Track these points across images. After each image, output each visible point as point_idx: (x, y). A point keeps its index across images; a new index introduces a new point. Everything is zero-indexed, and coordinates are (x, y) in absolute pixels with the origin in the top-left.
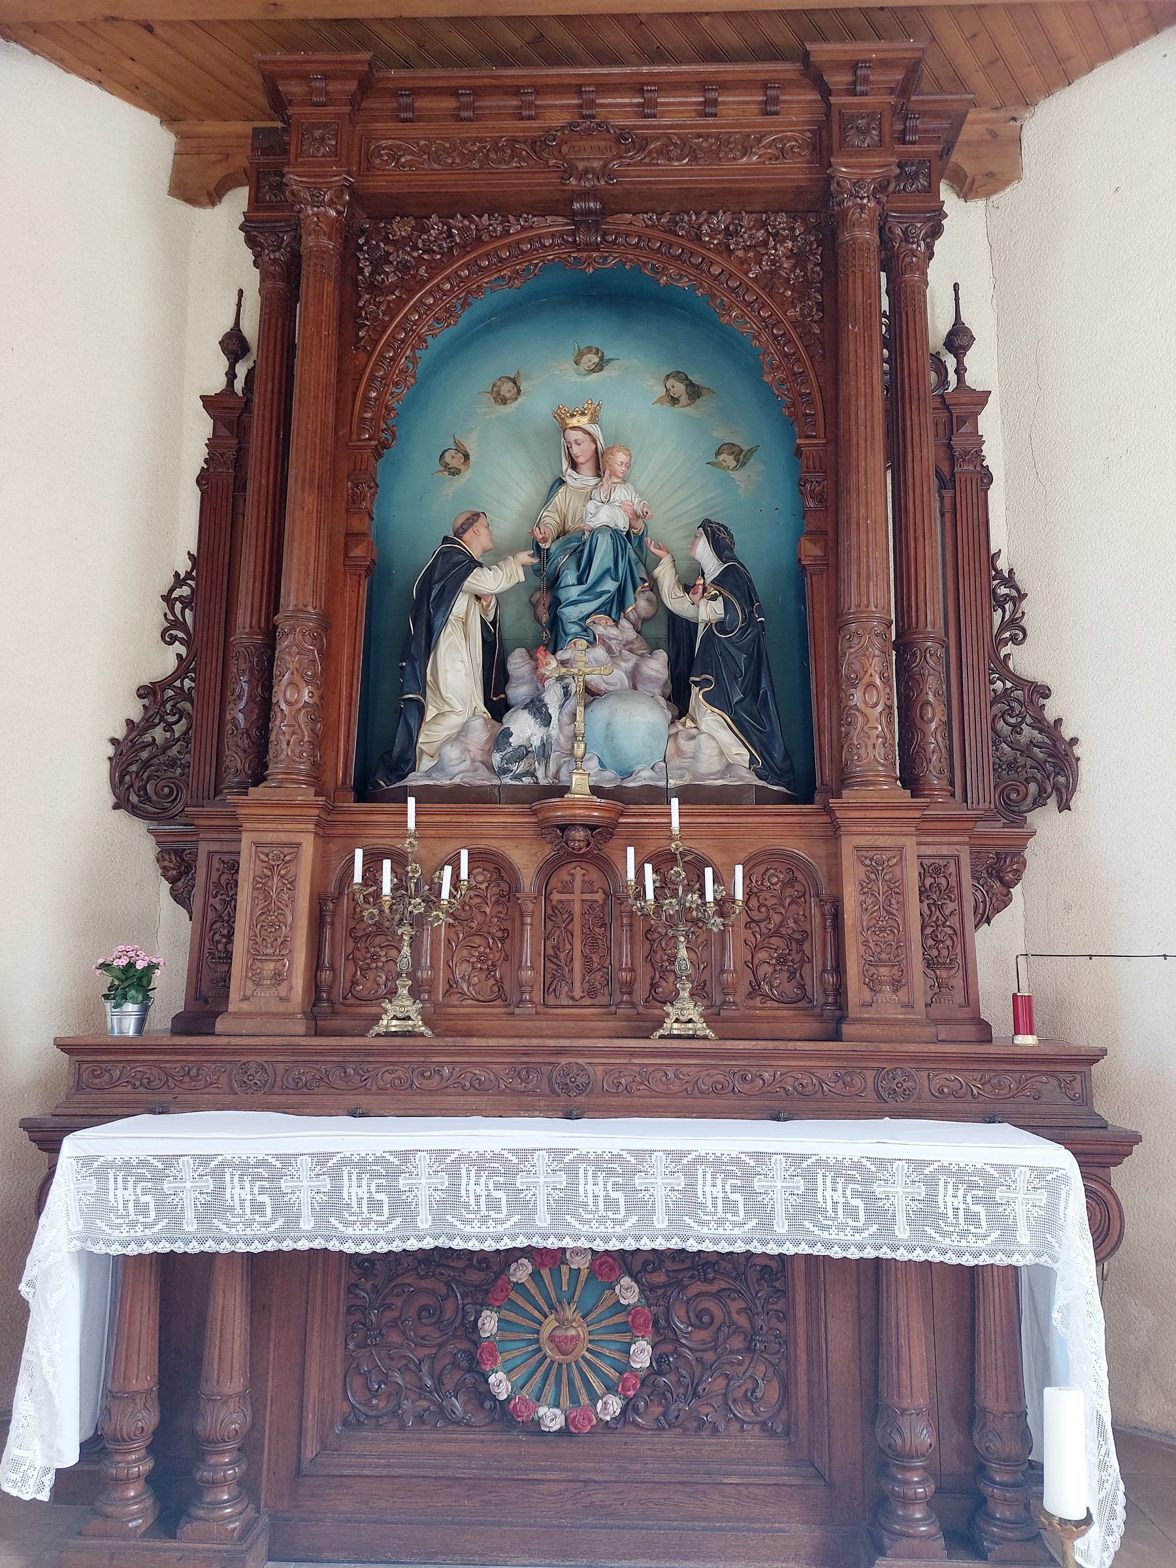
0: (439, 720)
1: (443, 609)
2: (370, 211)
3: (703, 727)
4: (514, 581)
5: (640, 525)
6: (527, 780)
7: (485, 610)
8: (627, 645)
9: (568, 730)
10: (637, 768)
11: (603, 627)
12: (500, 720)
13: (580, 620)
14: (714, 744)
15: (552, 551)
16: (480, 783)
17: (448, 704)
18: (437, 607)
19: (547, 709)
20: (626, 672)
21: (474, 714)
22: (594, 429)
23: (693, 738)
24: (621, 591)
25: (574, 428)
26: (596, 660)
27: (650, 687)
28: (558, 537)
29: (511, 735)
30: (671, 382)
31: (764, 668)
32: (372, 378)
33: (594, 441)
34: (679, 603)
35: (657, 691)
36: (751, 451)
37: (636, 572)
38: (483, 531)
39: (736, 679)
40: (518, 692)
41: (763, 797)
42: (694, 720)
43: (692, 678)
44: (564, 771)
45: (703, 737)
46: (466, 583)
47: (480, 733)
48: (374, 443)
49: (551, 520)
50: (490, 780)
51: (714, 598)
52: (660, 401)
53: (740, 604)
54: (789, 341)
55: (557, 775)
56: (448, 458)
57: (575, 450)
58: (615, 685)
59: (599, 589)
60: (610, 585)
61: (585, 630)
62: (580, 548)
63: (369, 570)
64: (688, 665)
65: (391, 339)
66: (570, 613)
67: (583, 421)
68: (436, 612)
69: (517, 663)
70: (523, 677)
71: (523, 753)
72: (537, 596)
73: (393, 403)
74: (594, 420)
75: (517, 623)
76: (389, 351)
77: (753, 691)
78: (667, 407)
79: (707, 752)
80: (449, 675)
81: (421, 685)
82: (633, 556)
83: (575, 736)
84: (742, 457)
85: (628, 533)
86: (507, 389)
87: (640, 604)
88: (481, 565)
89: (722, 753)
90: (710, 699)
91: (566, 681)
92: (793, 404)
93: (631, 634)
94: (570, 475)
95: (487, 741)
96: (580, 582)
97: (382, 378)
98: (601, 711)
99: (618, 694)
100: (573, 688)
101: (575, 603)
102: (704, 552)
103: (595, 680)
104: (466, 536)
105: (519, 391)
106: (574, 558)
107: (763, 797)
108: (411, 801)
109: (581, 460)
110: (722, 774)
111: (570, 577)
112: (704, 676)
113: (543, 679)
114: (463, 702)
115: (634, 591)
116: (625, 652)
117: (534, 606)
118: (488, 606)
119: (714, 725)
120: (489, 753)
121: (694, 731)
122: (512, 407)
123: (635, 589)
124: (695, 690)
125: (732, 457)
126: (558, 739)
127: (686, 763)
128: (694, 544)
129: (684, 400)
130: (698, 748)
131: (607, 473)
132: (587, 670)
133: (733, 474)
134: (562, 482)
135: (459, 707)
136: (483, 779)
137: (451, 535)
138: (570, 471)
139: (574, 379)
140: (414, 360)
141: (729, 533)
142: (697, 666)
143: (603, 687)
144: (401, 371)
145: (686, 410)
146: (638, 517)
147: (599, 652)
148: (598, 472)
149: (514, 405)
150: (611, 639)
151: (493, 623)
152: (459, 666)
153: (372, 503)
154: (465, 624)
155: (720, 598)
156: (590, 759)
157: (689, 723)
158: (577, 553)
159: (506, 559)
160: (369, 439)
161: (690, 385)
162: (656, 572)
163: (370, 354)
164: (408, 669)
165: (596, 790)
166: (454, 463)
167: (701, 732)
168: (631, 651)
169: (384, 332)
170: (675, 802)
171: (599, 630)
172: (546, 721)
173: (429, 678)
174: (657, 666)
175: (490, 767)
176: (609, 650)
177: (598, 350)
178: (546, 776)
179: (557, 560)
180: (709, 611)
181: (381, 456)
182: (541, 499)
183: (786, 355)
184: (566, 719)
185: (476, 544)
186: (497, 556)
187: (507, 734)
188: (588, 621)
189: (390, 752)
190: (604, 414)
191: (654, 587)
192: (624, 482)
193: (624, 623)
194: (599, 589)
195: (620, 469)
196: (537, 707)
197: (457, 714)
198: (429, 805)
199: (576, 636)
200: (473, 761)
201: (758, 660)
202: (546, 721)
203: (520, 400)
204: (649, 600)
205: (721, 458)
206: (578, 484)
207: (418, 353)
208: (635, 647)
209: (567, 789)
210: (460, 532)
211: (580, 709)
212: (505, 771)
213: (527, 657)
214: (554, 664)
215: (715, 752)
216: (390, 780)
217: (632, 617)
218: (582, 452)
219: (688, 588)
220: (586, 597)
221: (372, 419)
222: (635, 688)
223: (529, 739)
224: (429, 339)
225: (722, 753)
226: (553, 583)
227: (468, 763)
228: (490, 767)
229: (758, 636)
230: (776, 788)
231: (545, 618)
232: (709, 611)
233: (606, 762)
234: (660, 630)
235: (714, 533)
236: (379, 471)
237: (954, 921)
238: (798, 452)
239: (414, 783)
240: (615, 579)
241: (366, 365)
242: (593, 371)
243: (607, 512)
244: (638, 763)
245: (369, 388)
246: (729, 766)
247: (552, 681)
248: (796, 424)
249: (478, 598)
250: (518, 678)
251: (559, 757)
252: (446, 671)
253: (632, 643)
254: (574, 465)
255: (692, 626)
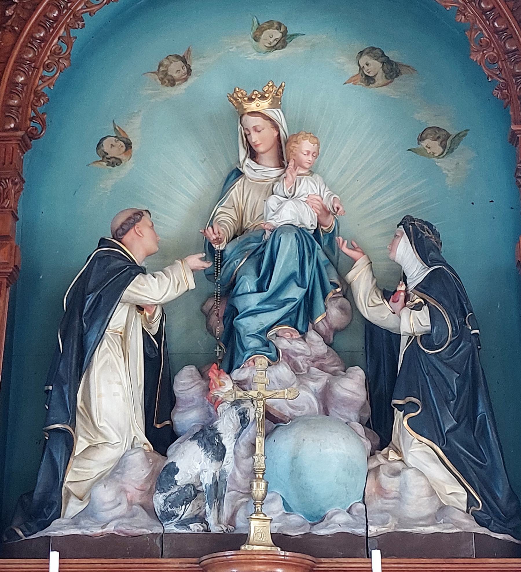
0: (91, 453)
1: (98, 323)
2: (272, 232)
3: (409, 460)
4: (182, 290)
5: (330, 221)
6: (195, 527)
7: (148, 322)
8: (317, 361)
9: (246, 464)
10: (330, 511)
11: (287, 341)
12: (164, 454)
13: (261, 332)
14: (423, 482)
15: (227, 253)
16: (137, 531)
17: (102, 434)
18: (91, 322)
19: (220, 440)
20: (315, 394)
21: (133, 446)
22: (276, 114)
23: (397, 473)
24: (309, 299)
25: (253, 113)
26: (279, 381)
27: (344, 411)
28: (235, 237)
29: (177, 471)
30: (365, 59)
31: (481, 390)
32: (20, 61)
33: (276, 127)
34: (377, 312)
35: (353, 416)
36: (460, 136)
37: (326, 276)
38: (147, 232)
39: (447, 402)
40: (186, 418)
41: (484, 548)
42: (398, 451)
43: (395, 401)
44: (241, 515)
45: (409, 473)
46: (126, 293)
47: (139, 469)
48: (20, 133)
49: (226, 217)
50: (149, 527)
51: (418, 307)
52: (352, 80)
53: (449, 314)
54: (499, 16)
55: (232, 521)
56: (106, 147)
57: (254, 138)
58: (302, 408)
59: (282, 297)
60: (295, 292)
61: (266, 344)
62: (259, 247)
63: (11, 278)
64: (390, 385)
65: (42, 18)
66: (249, 325)
67: (263, 106)
68: (90, 327)
69: (186, 383)
70: (193, 400)
71: (192, 493)
72: (210, 303)
73: (44, 88)
74: (276, 103)
75: (184, 335)
76: (39, 31)
77: (468, 416)
78: (360, 87)
79: (415, 491)
80: (104, 400)
81: (70, 414)
82: (323, 258)
83: (254, 472)
84: (449, 143)
85: (316, 231)
86: (175, 69)
87: (329, 314)
88: (143, 271)
89: (433, 493)
90: (416, 426)
91: (243, 406)
92: (507, 86)
93: (321, 348)
94: (248, 166)
95: (148, 480)
96: (260, 289)
97: (31, 60)
98: (285, 442)
99: (305, 420)
100: (251, 414)
101: (254, 313)
102: (405, 254)
103: (280, 405)
104: (127, 238)
105: (189, 71)
106: (253, 260)
107: (484, 548)
108: (54, 556)
109: (261, 149)
110: (434, 519)
111: (248, 283)
112: (408, 399)
113: (216, 402)
114: (120, 431)
115: (324, 297)
116: (314, 370)
117: (207, 316)
118: (152, 317)
119: (422, 458)
120: (150, 493)
121: (399, 465)
122: (180, 89)
123: (325, 297)
124: (398, 414)
125: (437, 143)
126: (234, 475)
127: (390, 504)
128: (393, 245)
129: (380, 79)
130: (403, 487)
131: (292, 163)
132: (268, 393)
133: (441, 163)
134: (239, 174)
135: (114, 438)
136: (142, 526)
137: (109, 236)
138: (248, 161)
139: (252, 57)
140: (68, 40)
141: (434, 231)
142: (401, 386)
143: (288, 411)
144: (53, 53)
145: (381, 90)
146: (329, 213)
147: (283, 371)
148: (281, 162)
149: (184, 86)
150: (296, 354)
151: (158, 336)
152: (117, 388)
153: (16, 200)
154: (124, 339)
155: (426, 308)
156: (272, 500)
157: (392, 456)
158: (256, 255)
159: (172, 264)
160: (15, 129)
161: (387, 62)
162: (350, 276)
163: (18, 35)
164: (55, 394)
165: (280, 540)
166: (113, 152)
167: (407, 467)
168: (321, 368)
169: (35, 10)
170: (376, 554)
171: (283, 344)
172: (219, 453)
173: (79, 403)
174: (352, 386)
175: (150, 511)
176: (295, 368)
177: (280, 24)
178: (219, 522)
179: (232, 263)
180: (413, 323)
181: (27, 147)
182: (215, 193)
183: (496, 31)
184: (243, 451)
185: (138, 246)
186: (164, 258)
187: (172, 470)
188: (270, 334)
189: (30, 494)
190: (288, 96)
191: (348, 293)
192: (311, 173)
193: (312, 335)
194: (282, 297)
195: (306, 159)
196: (208, 438)
197: (112, 446)
198: (75, 561)
199: (256, 351)
200: (131, 503)
201: (473, 380)
202: (219, 453)
203: (191, 80)
204: (342, 308)
205: (424, 144)
206: (258, 176)
207: (73, 33)
208: (326, 362)
209: (244, 538)
210: (119, 234)
211: (260, 440)
212: (169, 516)
213: (197, 376)
214: (229, 385)
215: (425, 491)
216: (29, 529)
217: (322, 327)
218: (264, 139)
219: (388, 295)
220: (267, 306)
221: (19, 107)
222: (326, 412)
223: (198, 476)
224: (86, 16)
225: (433, 493)
226: (229, 289)
227: (124, 506)
228: (150, 511)
229: (472, 351)
230: (500, 536)
231: (219, 329)
232: (413, 323)
233: (293, 502)
234: (356, 342)
235: (416, 232)
236: (26, 163)
237: (239, 260)
238: (514, 139)
239: (58, 533)
240: (301, 285)
241: (13, 46)
242: (274, 48)
243: (293, 208)
244: (330, 506)
245: (15, 72)
246: (442, 508)
247: (226, 406)
248: (510, 107)
249: (140, 309)
250: (186, 402)
251: (235, 498)
252: (100, 396)
253: (323, 358)
254: (253, 155)
255: (392, 338)
